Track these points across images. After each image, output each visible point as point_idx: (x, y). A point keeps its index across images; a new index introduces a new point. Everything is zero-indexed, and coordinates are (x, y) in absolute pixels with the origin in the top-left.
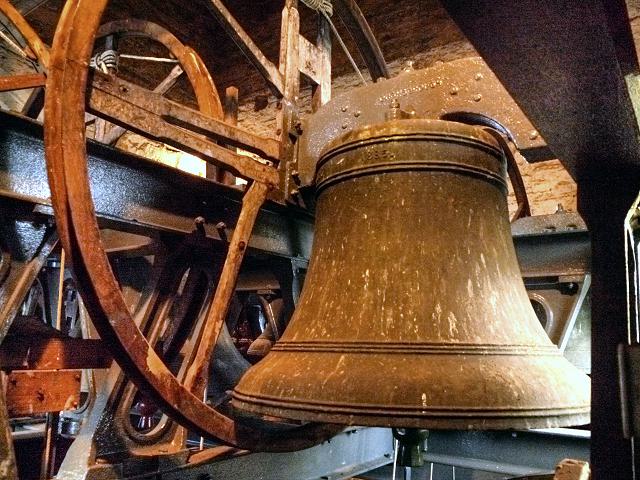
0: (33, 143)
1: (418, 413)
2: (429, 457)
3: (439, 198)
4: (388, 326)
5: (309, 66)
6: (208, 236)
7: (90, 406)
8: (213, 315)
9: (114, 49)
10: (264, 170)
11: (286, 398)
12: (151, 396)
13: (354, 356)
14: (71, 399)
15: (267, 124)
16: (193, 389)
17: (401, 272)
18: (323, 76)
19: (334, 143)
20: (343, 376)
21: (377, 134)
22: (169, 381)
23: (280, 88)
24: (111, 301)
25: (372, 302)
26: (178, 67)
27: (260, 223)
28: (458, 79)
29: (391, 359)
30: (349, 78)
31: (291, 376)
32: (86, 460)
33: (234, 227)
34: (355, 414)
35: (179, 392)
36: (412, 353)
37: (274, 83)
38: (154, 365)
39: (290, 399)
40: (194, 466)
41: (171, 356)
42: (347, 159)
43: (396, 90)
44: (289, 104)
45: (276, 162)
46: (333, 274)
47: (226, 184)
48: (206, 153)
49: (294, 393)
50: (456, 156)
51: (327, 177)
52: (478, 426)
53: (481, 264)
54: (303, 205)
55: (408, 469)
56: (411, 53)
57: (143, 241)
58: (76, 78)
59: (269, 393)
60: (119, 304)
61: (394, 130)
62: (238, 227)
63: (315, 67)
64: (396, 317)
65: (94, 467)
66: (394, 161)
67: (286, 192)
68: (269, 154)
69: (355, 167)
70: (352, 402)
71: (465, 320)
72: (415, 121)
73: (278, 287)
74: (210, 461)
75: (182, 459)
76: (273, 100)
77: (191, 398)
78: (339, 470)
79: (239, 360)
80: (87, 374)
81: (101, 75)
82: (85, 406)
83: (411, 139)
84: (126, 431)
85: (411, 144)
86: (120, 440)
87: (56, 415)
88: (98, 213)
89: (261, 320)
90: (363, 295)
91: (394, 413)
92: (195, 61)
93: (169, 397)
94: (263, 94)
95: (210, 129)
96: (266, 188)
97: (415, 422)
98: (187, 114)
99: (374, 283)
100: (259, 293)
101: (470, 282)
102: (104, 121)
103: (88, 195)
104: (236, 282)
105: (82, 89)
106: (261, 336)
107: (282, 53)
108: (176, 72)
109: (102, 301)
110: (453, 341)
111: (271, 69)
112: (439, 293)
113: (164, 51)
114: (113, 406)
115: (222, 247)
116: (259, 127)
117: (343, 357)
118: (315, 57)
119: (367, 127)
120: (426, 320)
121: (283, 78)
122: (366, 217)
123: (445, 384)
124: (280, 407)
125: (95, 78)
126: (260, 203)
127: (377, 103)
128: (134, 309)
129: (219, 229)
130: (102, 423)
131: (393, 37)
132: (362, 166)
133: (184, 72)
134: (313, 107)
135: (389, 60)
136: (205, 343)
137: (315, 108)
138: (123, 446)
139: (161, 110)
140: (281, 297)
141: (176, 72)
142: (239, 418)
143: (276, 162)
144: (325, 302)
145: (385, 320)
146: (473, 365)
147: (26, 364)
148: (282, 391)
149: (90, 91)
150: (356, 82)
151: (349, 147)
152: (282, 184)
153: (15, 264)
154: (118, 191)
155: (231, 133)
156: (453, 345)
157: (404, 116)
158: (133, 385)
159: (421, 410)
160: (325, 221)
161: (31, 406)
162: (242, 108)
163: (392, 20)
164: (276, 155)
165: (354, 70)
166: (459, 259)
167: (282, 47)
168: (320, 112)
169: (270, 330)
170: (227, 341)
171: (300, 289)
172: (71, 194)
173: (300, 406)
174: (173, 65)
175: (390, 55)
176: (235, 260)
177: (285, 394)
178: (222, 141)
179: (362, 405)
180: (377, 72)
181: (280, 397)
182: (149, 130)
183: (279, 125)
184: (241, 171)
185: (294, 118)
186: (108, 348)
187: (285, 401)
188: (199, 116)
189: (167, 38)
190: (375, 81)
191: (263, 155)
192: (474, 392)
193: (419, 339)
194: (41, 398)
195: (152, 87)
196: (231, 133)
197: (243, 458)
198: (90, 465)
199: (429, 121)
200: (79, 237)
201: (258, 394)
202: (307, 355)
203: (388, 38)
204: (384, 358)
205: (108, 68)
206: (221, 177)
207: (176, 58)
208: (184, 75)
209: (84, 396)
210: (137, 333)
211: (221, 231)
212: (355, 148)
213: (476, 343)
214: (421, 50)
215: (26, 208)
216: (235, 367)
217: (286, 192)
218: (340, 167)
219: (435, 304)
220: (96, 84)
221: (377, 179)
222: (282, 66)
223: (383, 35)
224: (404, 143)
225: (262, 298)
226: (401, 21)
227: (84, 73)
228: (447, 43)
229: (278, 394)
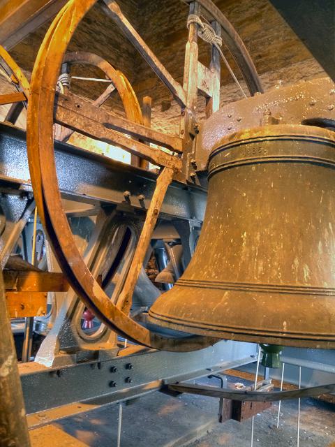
0: (19, 143)
1: (280, 335)
2: (282, 359)
3: (299, 182)
4: (259, 272)
5: (204, 83)
6: (132, 205)
8: (136, 259)
9: (68, 73)
10: (172, 159)
11: (186, 319)
13: (235, 292)
14: (41, 309)
15: (170, 120)
17: (269, 235)
18: (214, 92)
19: (223, 140)
20: (226, 307)
21: (255, 135)
22: (107, 303)
23: (183, 100)
24: (70, 250)
25: (248, 255)
26: (111, 85)
28: (316, 93)
29: (261, 296)
30: (231, 87)
31: (190, 304)
32: (53, 352)
33: (150, 198)
34: (235, 333)
36: (276, 293)
37: (179, 96)
38: (97, 292)
39: (190, 320)
40: (122, 358)
41: (105, 283)
42: (232, 153)
43: (269, 102)
44: (190, 112)
45: (180, 153)
46: (220, 234)
47: (144, 168)
48: (133, 149)
49: (192, 316)
50: (312, 152)
51: (216, 165)
52: (324, 346)
53: (329, 230)
54: (198, 184)
55: (267, 369)
56: (277, 67)
57: (89, 207)
58: (47, 100)
59: (175, 314)
61: (267, 133)
62: (154, 199)
63: (208, 85)
64: (265, 266)
65: (58, 356)
66: (266, 155)
67: (187, 174)
68: (175, 148)
70: (232, 324)
71: (316, 270)
72: (283, 126)
73: (179, 237)
74: (133, 355)
75: (114, 353)
76: (174, 103)
77: (122, 315)
78: (219, 365)
79: (151, 287)
80: (51, 295)
81: (63, 96)
82: (50, 313)
83: (280, 139)
84: (78, 334)
85: (280, 142)
86: (74, 339)
87: (32, 319)
88: (61, 190)
89: (164, 258)
90: (242, 250)
91: (263, 334)
92: (123, 81)
94: (167, 100)
96: (173, 172)
97: (278, 341)
98: (120, 122)
99: (250, 242)
100: (164, 240)
101: (320, 243)
102: (60, 126)
103: (55, 180)
104: (152, 234)
105: (51, 107)
106: (165, 270)
107: (185, 76)
108: (110, 89)
110: (306, 285)
111: (177, 87)
112: (297, 250)
113: (102, 74)
114: (70, 317)
115: (142, 213)
116: (165, 126)
117: (226, 293)
118: (208, 77)
119: (247, 130)
120: (287, 269)
121: (186, 93)
122: (245, 195)
123: (301, 316)
124: (183, 325)
125: (59, 98)
126: (169, 183)
127: (254, 111)
129: (140, 200)
130: (63, 327)
131: (264, 56)
132: (242, 159)
133: (116, 89)
134: (206, 113)
135: (260, 73)
136: (131, 278)
137: (208, 116)
138: (75, 342)
139: (103, 119)
140: (180, 244)
141: (110, 89)
142: (152, 328)
143: (180, 153)
144: (214, 254)
145: (257, 268)
146: (321, 303)
147: (15, 288)
148: (184, 314)
149: (57, 108)
150: (235, 90)
151: (234, 144)
153: (8, 223)
154: (73, 175)
155: (150, 134)
156: (306, 288)
157: (275, 122)
158: (83, 304)
159: (283, 333)
160: (215, 197)
161: (16, 313)
162: (153, 109)
163: (262, 44)
164: (180, 148)
165: (234, 81)
166: (313, 226)
167: (185, 71)
168: (212, 117)
169: (171, 266)
171: (196, 241)
172: (44, 179)
173: (197, 325)
174: (109, 84)
175: (261, 70)
176: (151, 222)
177: (186, 316)
178: (142, 139)
179: (240, 327)
180: (254, 88)
181: (182, 318)
183: (183, 128)
184: (156, 160)
185: (194, 122)
186: (68, 278)
187: (186, 321)
188: (128, 123)
189: (104, 65)
190: (252, 95)
191: (170, 148)
192: (322, 322)
193: (282, 283)
194: (23, 308)
195: (95, 98)
196: (150, 134)
198: (55, 354)
199: (293, 126)
200: (49, 207)
201: (167, 315)
202: (201, 290)
203: (260, 57)
204: (256, 295)
205: (64, 86)
206: (140, 163)
207: (110, 79)
208: (116, 90)
209: (49, 307)
210: (87, 271)
211: (141, 201)
213: (324, 287)
214: (284, 65)
215: (14, 186)
216: (148, 291)
217: (187, 174)
218: (227, 159)
219: (294, 258)
221: (254, 168)
222: (185, 85)
223: (257, 54)
224: (274, 142)
225: (166, 244)
226: (270, 44)
227: (53, 96)
228: (305, 60)
229: (181, 316)
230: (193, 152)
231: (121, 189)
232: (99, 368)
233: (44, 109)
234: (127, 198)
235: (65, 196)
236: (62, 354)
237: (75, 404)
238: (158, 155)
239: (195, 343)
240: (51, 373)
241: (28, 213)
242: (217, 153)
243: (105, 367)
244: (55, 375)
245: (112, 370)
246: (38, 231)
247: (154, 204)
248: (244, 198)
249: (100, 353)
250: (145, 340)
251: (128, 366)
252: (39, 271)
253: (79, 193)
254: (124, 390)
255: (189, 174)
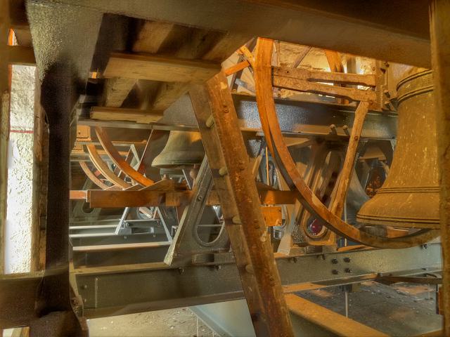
6: (338, 134)
7: (287, 224)
12: (318, 221)
16: (336, 213)
22: (323, 209)
27: (367, 120)
35: (329, 215)
41: (325, 199)
57: (305, 140)
60: (297, 174)
69: (416, 89)
80: (284, 206)
93: (324, 217)
95: (332, 79)
96: (368, 104)
103: (278, 126)
105: (270, 77)
109: (289, 173)
114: (298, 221)
115: (346, 139)
117: (411, 195)
128: (304, 174)
132: (420, 88)
143: (374, 87)
152: (378, 99)
170: (360, 190)
172: (271, 127)
182: (301, 89)
186: (293, 194)
197: (370, 252)
209: (283, 221)
211: (345, 130)
212: (416, 77)
218: (408, 89)
220: (275, 73)
225: (382, 162)
230: (385, 84)
231: (329, 124)
232: (324, 259)
233: (265, 81)
234: (333, 129)
235: (285, 135)
236: (296, 247)
237: (308, 283)
238: (353, 93)
239: (404, 242)
240: (289, 259)
241: (263, 150)
242: (402, 84)
243: (329, 258)
244: (292, 262)
245: (334, 262)
246: (270, 162)
247: (355, 130)
248: (423, 119)
249: (323, 248)
250: (356, 236)
251: (347, 260)
252: (274, 190)
253: (296, 132)
254: (346, 278)
255: (384, 102)
